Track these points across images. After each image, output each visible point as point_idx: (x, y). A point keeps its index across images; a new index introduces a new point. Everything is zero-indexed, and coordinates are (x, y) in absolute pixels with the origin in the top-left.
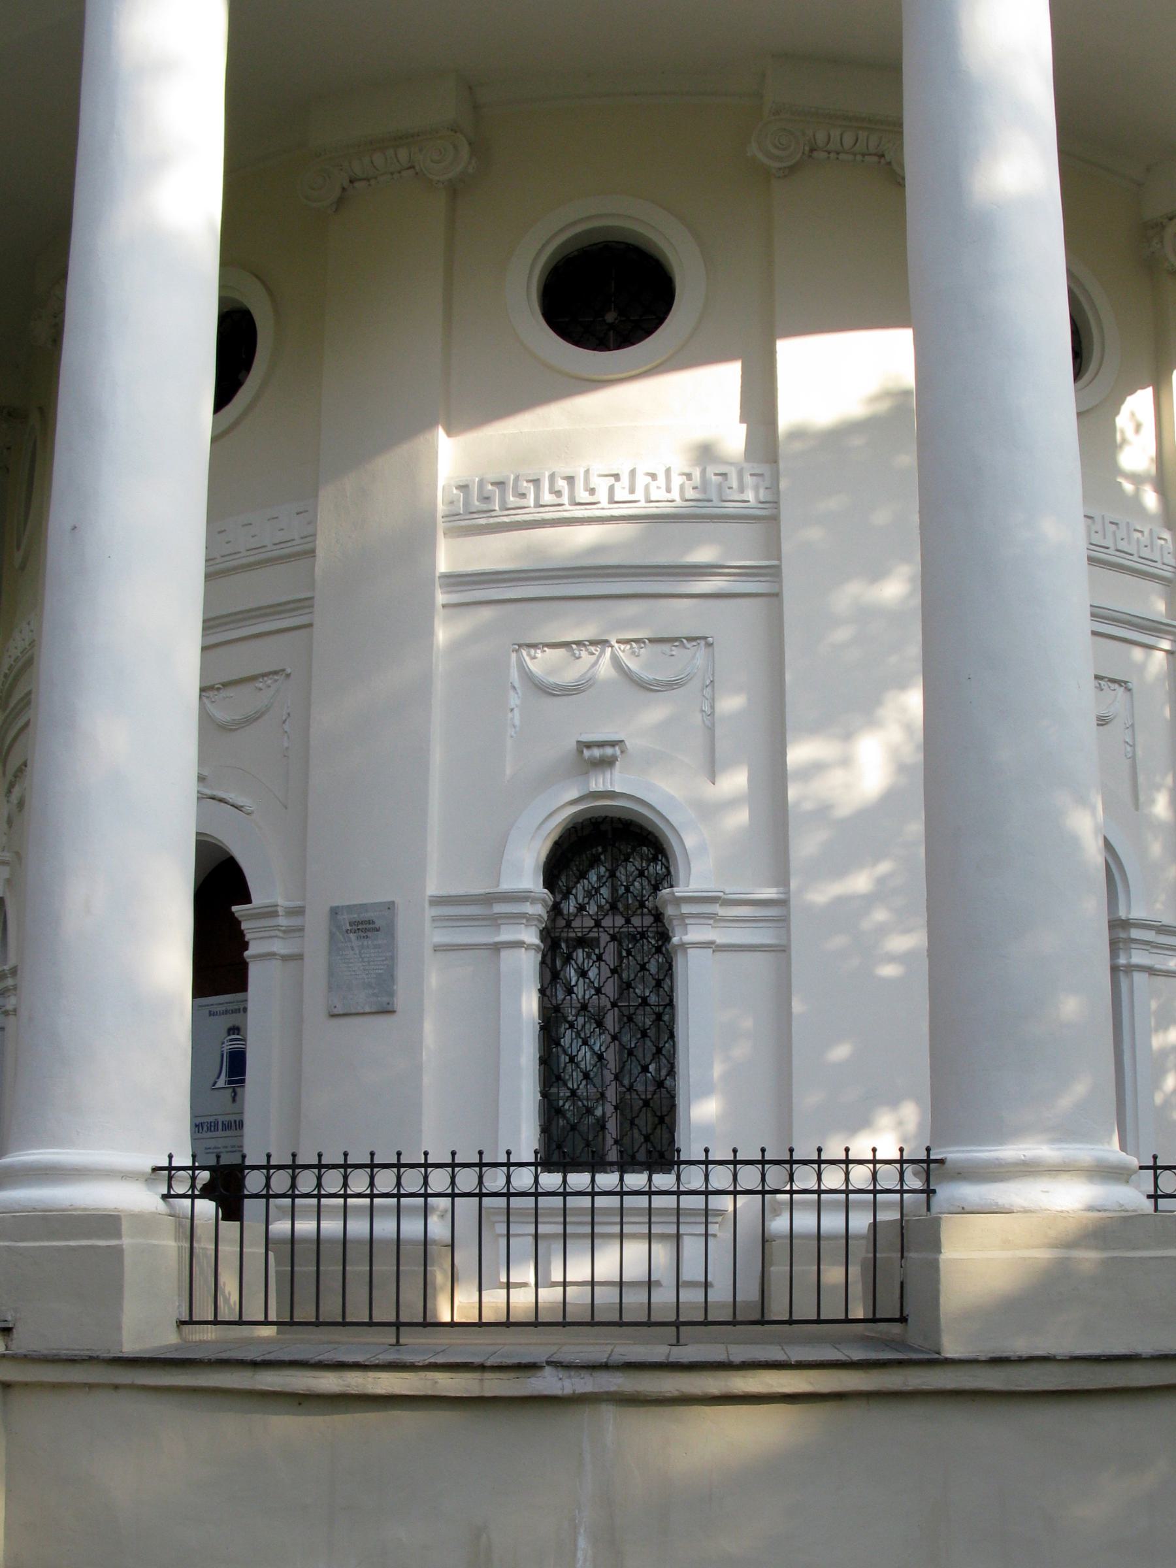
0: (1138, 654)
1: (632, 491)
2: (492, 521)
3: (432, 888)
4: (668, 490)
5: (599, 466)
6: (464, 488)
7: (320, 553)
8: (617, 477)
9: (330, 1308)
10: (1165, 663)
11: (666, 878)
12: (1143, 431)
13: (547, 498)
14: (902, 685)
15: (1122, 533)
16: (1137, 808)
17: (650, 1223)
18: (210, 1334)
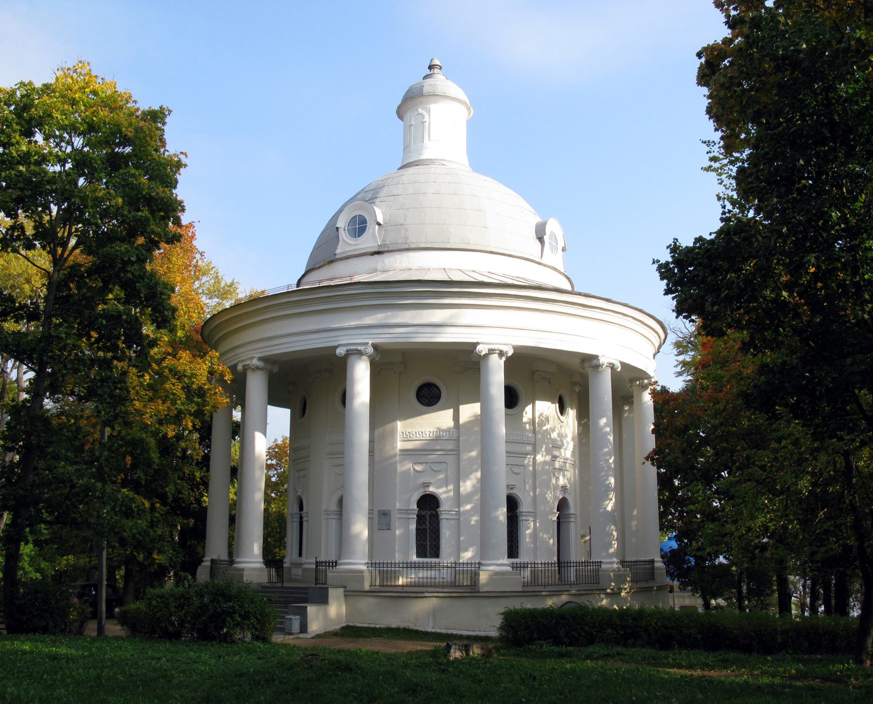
11: (438, 506)
14: (476, 471)
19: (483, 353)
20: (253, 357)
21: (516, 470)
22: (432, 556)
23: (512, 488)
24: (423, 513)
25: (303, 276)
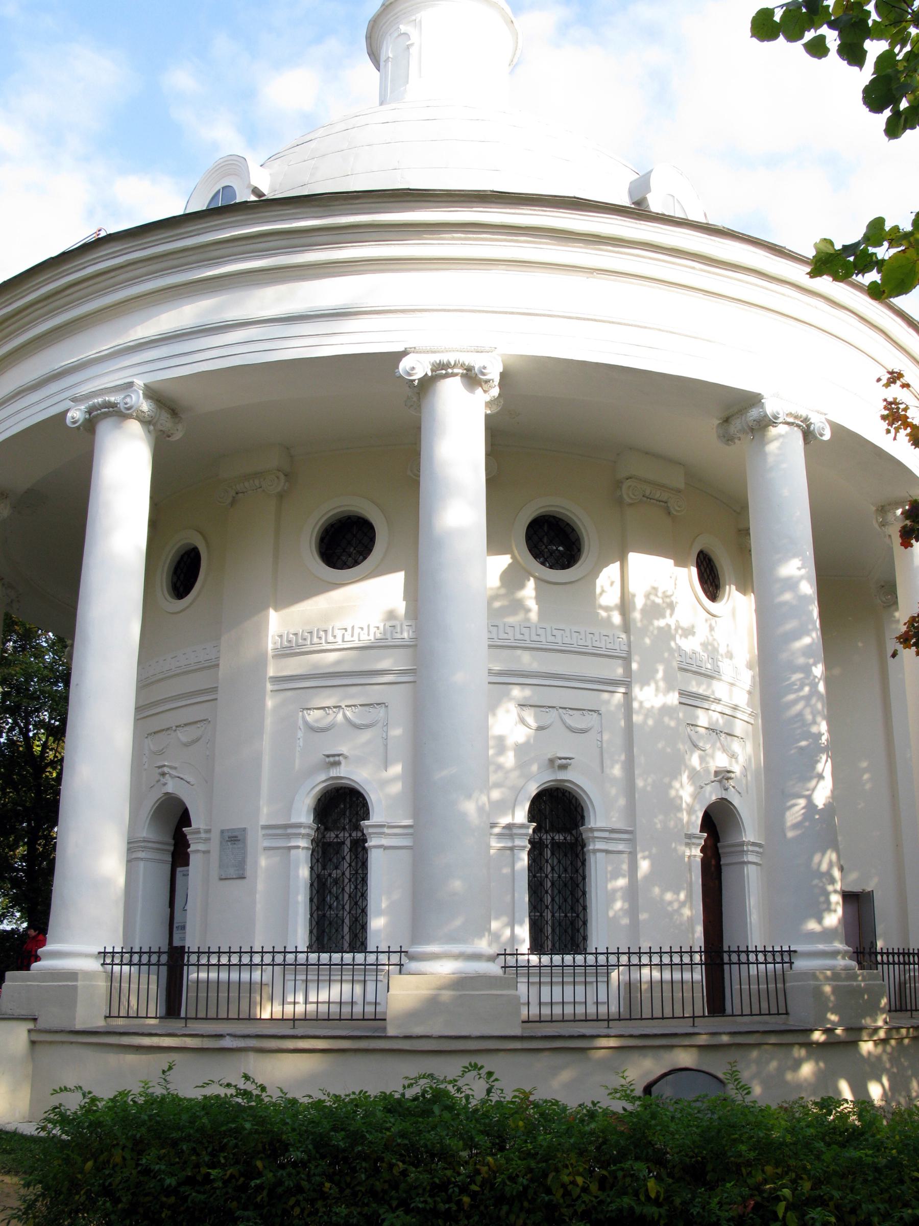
0: (606, 696)
1: (352, 636)
2: (292, 651)
3: (263, 821)
4: (369, 635)
5: (338, 624)
6: (281, 636)
7: (221, 666)
8: (346, 629)
9: (211, 1013)
10: (622, 700)
11: (366, 816)
12: (615, 585)
13: (315, 640)
15: (596, 637)
16: (603, 772)
17: (353, 975)
18: (120, 1022)
19: (418, 375)
21: (576, 721)
23: (563, 767)
24: (331, 836)
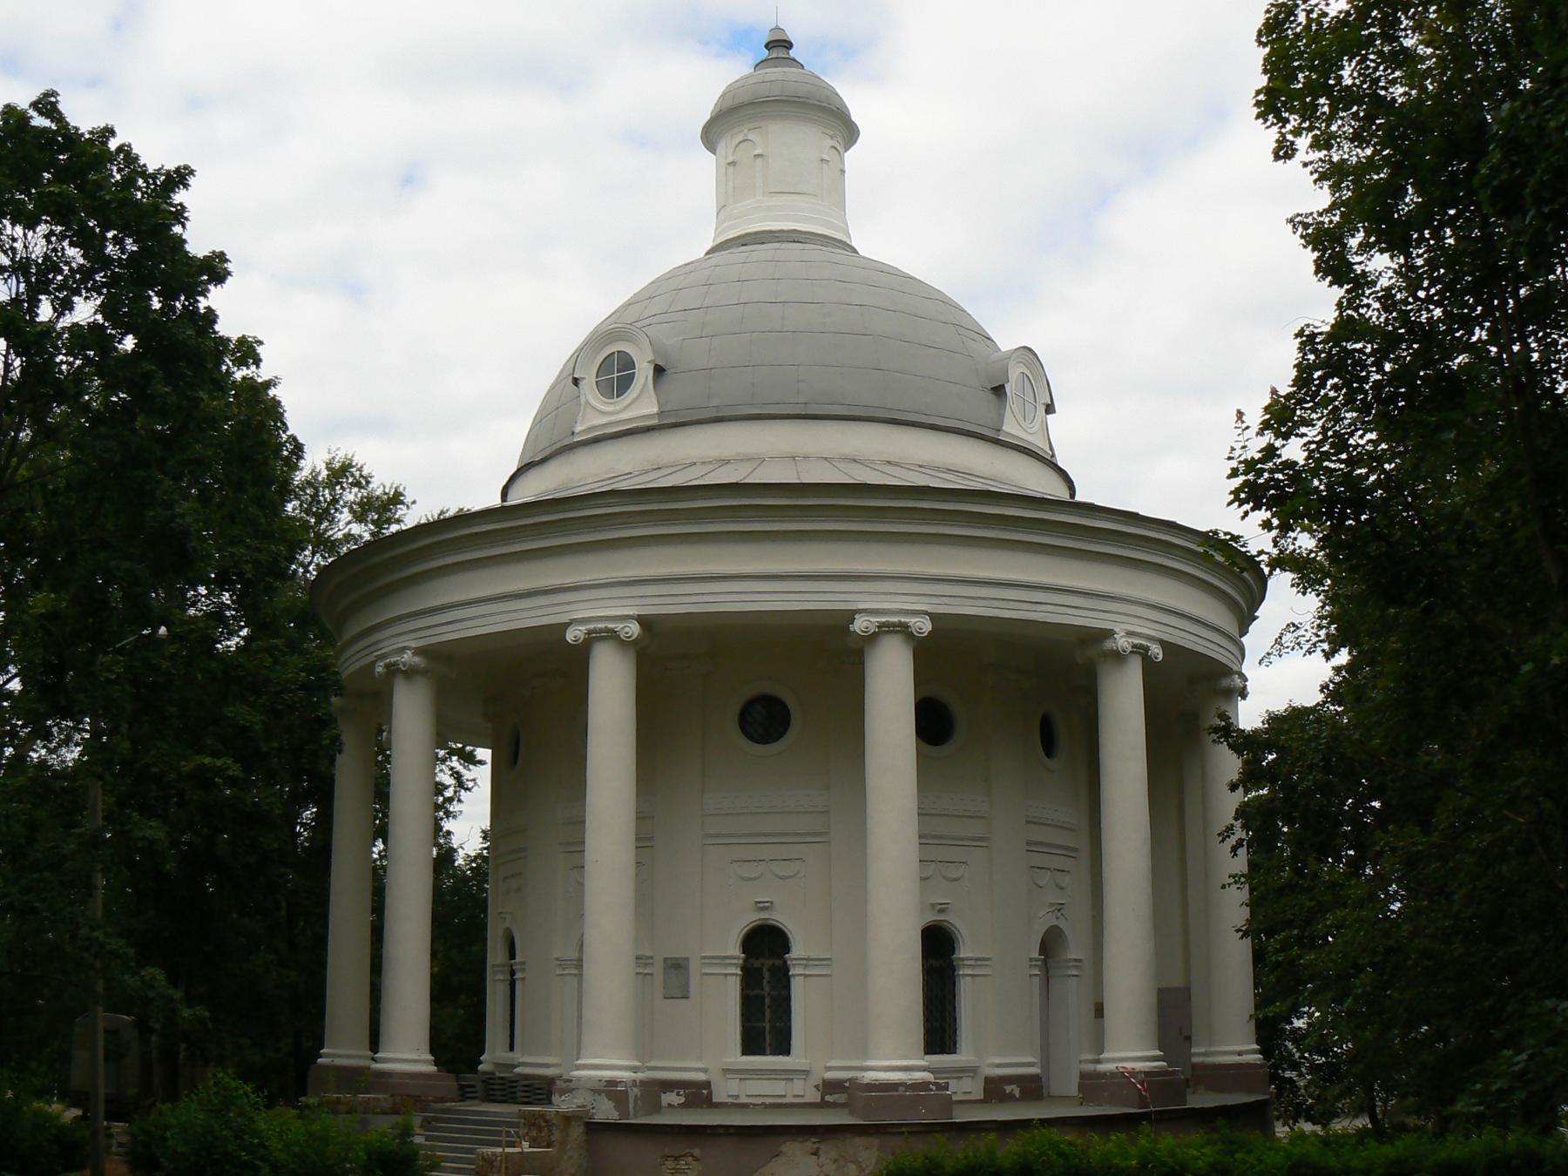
11: (788, 950)
20: (404, 649)
22: (776, 1052)
24: (757, 964)
25: (513, 479)
